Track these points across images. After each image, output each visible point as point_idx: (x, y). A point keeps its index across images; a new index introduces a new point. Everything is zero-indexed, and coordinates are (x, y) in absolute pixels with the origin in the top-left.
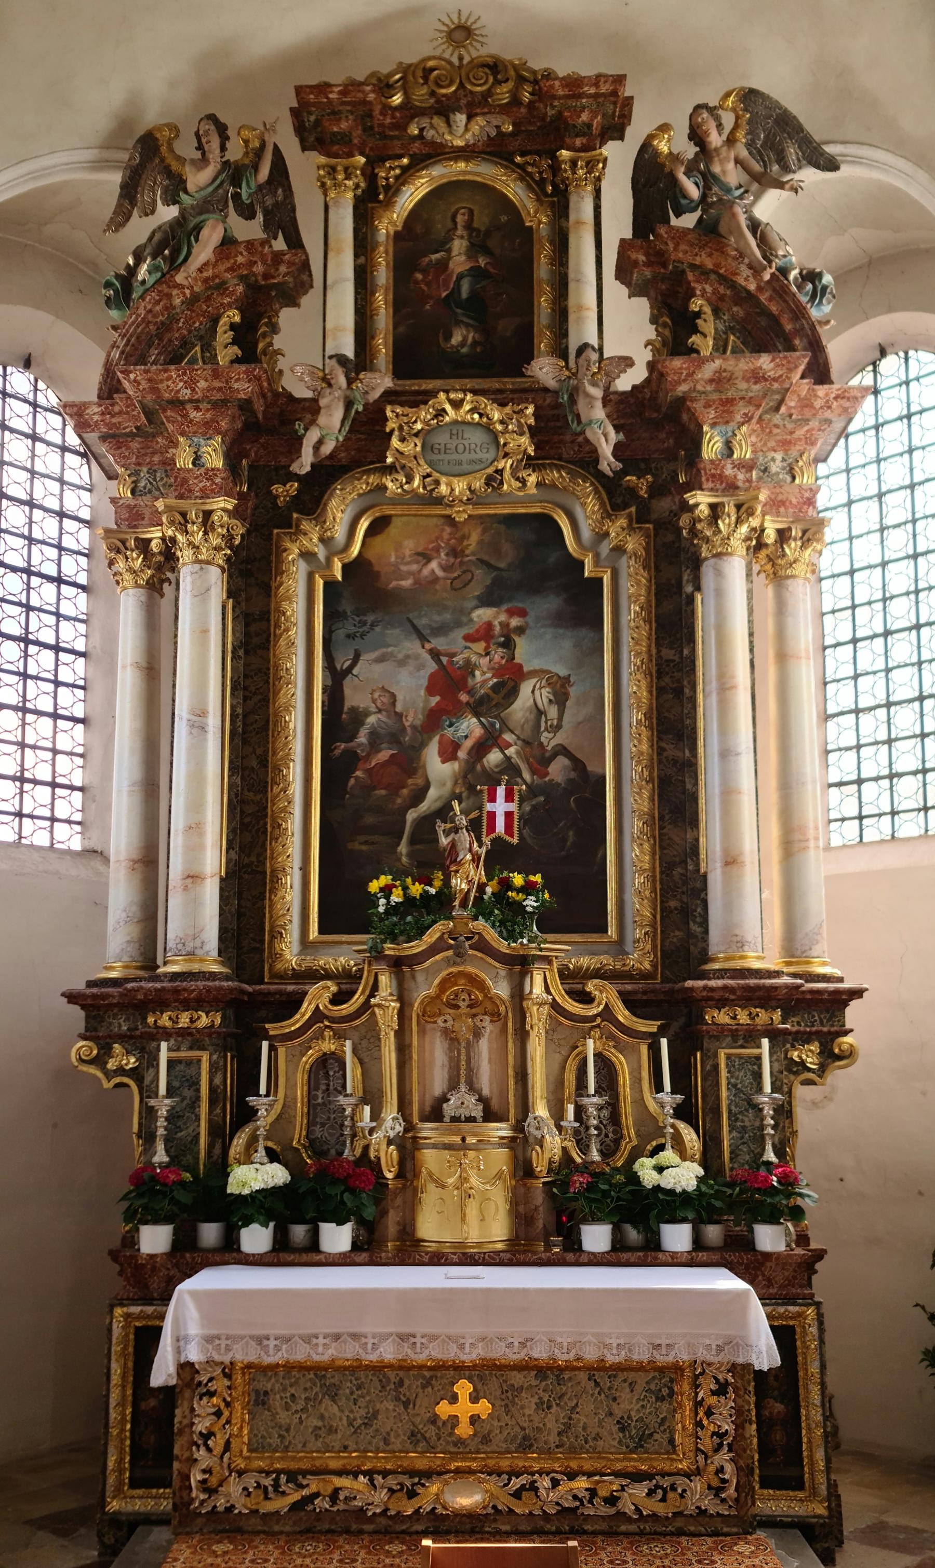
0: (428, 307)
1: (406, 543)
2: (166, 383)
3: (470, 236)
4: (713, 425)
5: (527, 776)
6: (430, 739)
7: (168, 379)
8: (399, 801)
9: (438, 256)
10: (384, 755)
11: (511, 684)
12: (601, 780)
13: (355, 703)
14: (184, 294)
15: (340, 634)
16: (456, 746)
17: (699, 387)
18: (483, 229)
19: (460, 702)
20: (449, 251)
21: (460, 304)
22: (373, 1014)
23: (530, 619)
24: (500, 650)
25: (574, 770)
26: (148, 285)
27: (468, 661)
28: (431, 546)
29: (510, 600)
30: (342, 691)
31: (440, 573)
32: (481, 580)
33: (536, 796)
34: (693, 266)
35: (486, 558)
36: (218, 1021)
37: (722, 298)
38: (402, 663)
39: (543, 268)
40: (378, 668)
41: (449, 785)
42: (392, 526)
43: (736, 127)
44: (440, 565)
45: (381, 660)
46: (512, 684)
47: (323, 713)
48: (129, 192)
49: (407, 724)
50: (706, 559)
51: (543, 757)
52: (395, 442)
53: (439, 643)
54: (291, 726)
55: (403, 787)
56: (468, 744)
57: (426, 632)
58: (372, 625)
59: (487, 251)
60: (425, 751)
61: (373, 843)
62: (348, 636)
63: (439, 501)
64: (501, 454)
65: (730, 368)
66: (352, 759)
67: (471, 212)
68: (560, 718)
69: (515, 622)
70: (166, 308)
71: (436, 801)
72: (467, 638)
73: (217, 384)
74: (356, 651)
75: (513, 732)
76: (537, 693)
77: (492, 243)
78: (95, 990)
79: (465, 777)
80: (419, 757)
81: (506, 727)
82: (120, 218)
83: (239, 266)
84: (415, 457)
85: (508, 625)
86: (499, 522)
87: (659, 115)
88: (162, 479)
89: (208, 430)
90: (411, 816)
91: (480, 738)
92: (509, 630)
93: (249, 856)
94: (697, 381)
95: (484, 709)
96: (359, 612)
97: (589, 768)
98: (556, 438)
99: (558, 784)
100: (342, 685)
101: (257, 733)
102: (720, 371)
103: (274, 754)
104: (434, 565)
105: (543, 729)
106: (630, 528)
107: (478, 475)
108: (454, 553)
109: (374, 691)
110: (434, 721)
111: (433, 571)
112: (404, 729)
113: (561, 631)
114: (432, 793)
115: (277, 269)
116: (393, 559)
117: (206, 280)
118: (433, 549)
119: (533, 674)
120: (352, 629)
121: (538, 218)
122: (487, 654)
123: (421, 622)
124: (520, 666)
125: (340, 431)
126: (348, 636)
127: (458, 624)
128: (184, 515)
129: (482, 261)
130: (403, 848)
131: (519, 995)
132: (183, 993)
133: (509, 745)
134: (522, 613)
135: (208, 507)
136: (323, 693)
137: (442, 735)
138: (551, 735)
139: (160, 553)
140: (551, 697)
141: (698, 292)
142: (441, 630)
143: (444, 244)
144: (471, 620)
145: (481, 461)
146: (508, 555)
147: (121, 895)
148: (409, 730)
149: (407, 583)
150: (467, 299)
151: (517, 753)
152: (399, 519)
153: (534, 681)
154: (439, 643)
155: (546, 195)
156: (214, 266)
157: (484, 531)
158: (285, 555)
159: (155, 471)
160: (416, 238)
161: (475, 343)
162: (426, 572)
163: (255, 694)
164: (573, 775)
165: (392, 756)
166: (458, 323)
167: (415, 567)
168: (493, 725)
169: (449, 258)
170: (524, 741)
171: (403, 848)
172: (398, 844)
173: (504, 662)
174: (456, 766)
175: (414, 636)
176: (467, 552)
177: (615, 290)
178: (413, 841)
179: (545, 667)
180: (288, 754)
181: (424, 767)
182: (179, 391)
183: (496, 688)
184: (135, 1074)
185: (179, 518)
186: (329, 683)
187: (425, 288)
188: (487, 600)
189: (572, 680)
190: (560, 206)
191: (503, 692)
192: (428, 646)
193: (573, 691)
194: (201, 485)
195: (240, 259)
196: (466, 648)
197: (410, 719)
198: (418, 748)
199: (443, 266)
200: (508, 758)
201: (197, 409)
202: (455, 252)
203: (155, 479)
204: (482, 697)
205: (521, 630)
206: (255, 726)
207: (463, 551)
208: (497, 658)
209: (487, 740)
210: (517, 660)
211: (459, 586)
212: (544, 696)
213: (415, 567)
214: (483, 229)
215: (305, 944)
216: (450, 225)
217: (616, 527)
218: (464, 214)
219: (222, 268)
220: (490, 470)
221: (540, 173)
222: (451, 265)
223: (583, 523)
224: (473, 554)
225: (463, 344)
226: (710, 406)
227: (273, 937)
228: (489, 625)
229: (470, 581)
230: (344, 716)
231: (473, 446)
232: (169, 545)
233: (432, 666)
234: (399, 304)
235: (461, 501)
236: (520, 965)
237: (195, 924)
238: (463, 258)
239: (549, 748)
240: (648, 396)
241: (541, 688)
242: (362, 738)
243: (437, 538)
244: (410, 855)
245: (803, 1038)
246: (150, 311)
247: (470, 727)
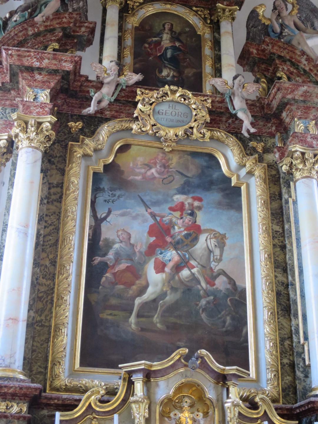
0: (151, 58)
1: (138, 158)
2: (27, 58)
3: (171, 34)
4: (300, 118)
5: (203, 284)
6: (150, 260)
7: (28, 56)
8: (131, 292)
9: (156, 39)
10: (123, 266)
11: (194, 235)
12: (244, 291)
13: (107, 236)
14: (34, 30)
15: (100, 199)
16: (164, 265)
17: (296, 98)
18: (177, 32)
19: (167, 242)
20: (162, 38)
21: (166, 59)
22: (130, 408)
23: (204, 203)
24: (188, 217)
25: (229, 283)
26: (17, 22)
27: (171, 221)
28: (152, 161)
29: (194, 192)
30: (101, 229)
31: (156, 175)
32: (179, 181)
33: (209, 296)
34: (280, 57)
35: (181, 171)
36: (25, 409)
37: (292, 73)
38: (135, 218)
39: (207, 51)
40: (121, 220)
41: (160, 286)
42: (131, 149)
43: (293, 10)
44: (157, 171)
45: (123, 215)
46: (195, 235)
47: (89, 240)
49: (137, 250)
50: (298, 179)
51: (212, 275)
52: (140, 106)
53: (155, 210)
54: (72, 242)
55: (133, 285)
56: (171, 265)
57: (148, 203)
58: (119, 197)
59: (179, 41)
60: (146, 266)
61: (115, 315)
62: (105, 201)
63: (159, 139)
64: (193, 120)
65: (311, 91)
66: (104, 267)
67: (172, 25)
68: (221, 255)
69: (196, 204)
70: (24, 35)
71: (152, 294)
72: (171, 209)
73: (54, 62)
74: (109, 209)
75: (195, 260)
76: (208, 241)
77: (183, 38)
79: (169, 282)
80: (143, 269)
81: (191, 257)
83: (63, 23)
84: (149, 115)
85: (192, 205)
86: (188, 155)
88: (9, 113)
89: (43, 85)
90: (138, 301)
91: (177, 262)
92: (193, 208)
93: (40, 316)
94: (295, 95)
95: (180, 246)
96: (112, 189)
97: (237, 283)
99: (221, 291)
100: (100, 226)
101: (50, 247)
102: (306, 92)
103: (61, 258)
104: (153, 171)
105: (212, 260)
106: (255, 164)
107: (180, 129)
108: (165, 166)
109: (118, 231)
110: (151, 250)
111: (153, 173)
112: (134, 253)
113: (221, 211)
114: (150, 290)
115: (80, 29)
116: (131, 165)
117: (46, 26)
118: (152, 163)
119: (206, 231)
120: (107, 198)
121: (205, 32)
122: (182, 218)
123: (146, 198)
124: (199, 227)
125: (112, 96)
126: (105, 201)
127: (166, 201)
128: (26, 123)
129: (177, 44)
130: (133, 319)
133: (193, 267)
134: (200, 200)
135: (40, 120)
136: (90, 229)
137: (156, 259)
138: (216, 264)
139: (4, 147)
140: (216, 244)
141: (280, 69)
142: (157, 203)
143: (159, 34)
144: (173, 200)
145: (183, 121)
146: (193, 171)
148: (138, 254)
149: (139, 178)
150: (170, 58)
151: (198, 271)
152: (136, 146)
153: (206, 235)
154: (155, 210)
155: (207, 23)
156: (52, 20)
157: (180, 158)
158: (75, 154)
159: (6, 109)
161: (174, 76)
162: (149, 173)
163: (51, 225)
164: (229, 286)
165: (128, 267)
166: (166, 67)
167: (143, 171)
168: (185, 256)
169: (161, 40)
170: (202, 265)
171: (133, 319)
172: (130, 317)
173: (190, 223)
174: (164, 275)
175: (142, 205)
176: (171, 167)
178: (139, 316)
179: (213, 229)
180: (70, 258)
181: (146, 275)
182: (33, 63)
183: (187, 236)
185: (23, 125)
186: (93, 224)
187: (150, 51)
188: (182, 191)
189: (227, 236)
190: (216, 27)
191: (190, 239)
192: (149, 211)
193: (228, 242)
194: (37, 110)
195: (64, 20)
196: (170, 214)
197: (138, 248)
198: (143, 264)
199: (159, 43)
200: (193, 274)
201: (40, 74)
202: (164, 38)
203: (5, 113)
204: (179, 240)
205: (199, 208)
206: (50, 242)
207: (168, 166)
208: (187, 221)
209: (181, 263)
210: (198, 223)
211: (167, 181)
212: (212, 243)
213: (143, 171)
214: (177, 32)
215: (73, 373)
216: (162, 28)
217: (250, 163)
218: (168, 25)
219: (55, 22)
220: (187, 127)
221: (205, 15)
222: (162, 43)
223: (230, 159)
224: (174, 168)
225: (168, 76)
226: (299, 109)
227: (54, 364)
228: (182, 204)
229: (172, 181)
230: (101, 243)
231: (180, 113)
233: (151, 221)
235: (171, 140)
238: (168, 41)
239: (215, 271)
240: (266, 103)
241: (210, 239)
242: (111, 255)
243: (155, 158)
244: (137, 324)
246: (16, 34)
247: (171, 256)
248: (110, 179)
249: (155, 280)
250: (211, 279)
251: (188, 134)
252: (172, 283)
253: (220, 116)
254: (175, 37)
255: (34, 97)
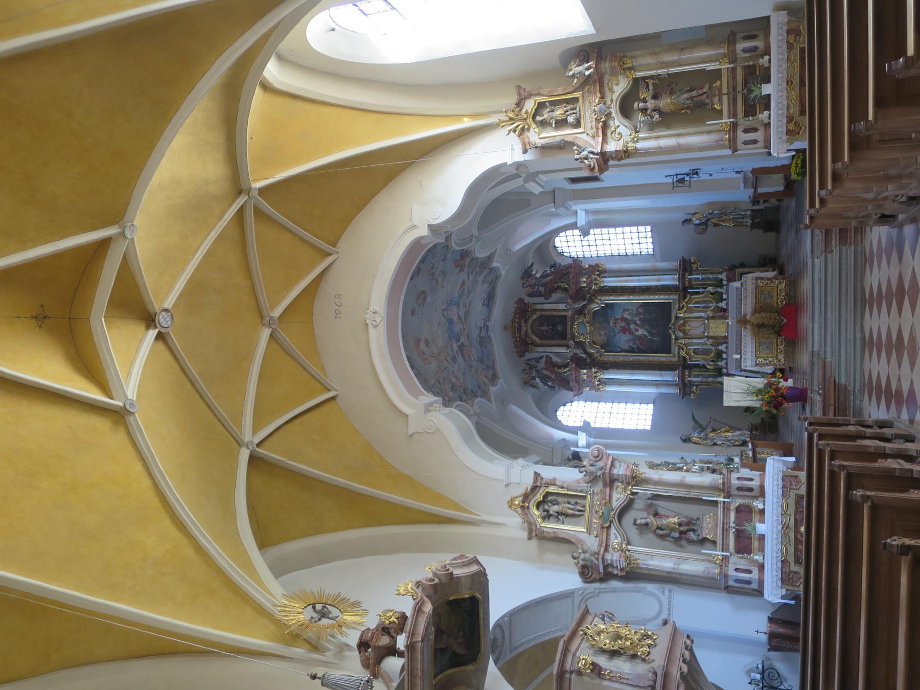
39: (548, 313)
48: (534, 387)
66: (638, 348)
78: (737, 585)
82: (538, 388)
87: (522, 293)
98: (580, 312)
110: (631, 333)
121: (538, 313)
131: (682, 318)
132: (682, 378)
147: (664, 390)
160: (542, 336)
177: (550, 300)
184: (697, 386)
215: (674, 356)
223: (595, 307)
232: (599, 381)
234: (553, 339)
236: (677, 318)
237: (668, 376)
245: (691, 268)
248: (607, 346)
249: (641, 332)
250: (639, 314)
251: (588, 322)
252: (642, 326)
253: (580, 312)
254: (542, 325)
255: (450, 386)
